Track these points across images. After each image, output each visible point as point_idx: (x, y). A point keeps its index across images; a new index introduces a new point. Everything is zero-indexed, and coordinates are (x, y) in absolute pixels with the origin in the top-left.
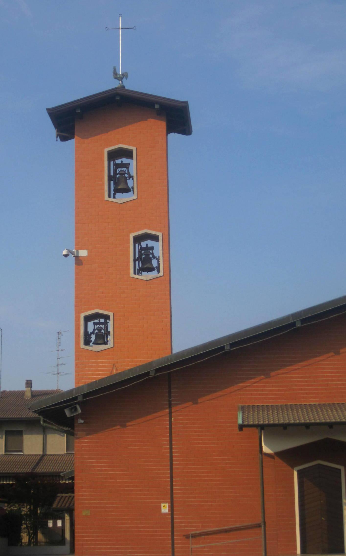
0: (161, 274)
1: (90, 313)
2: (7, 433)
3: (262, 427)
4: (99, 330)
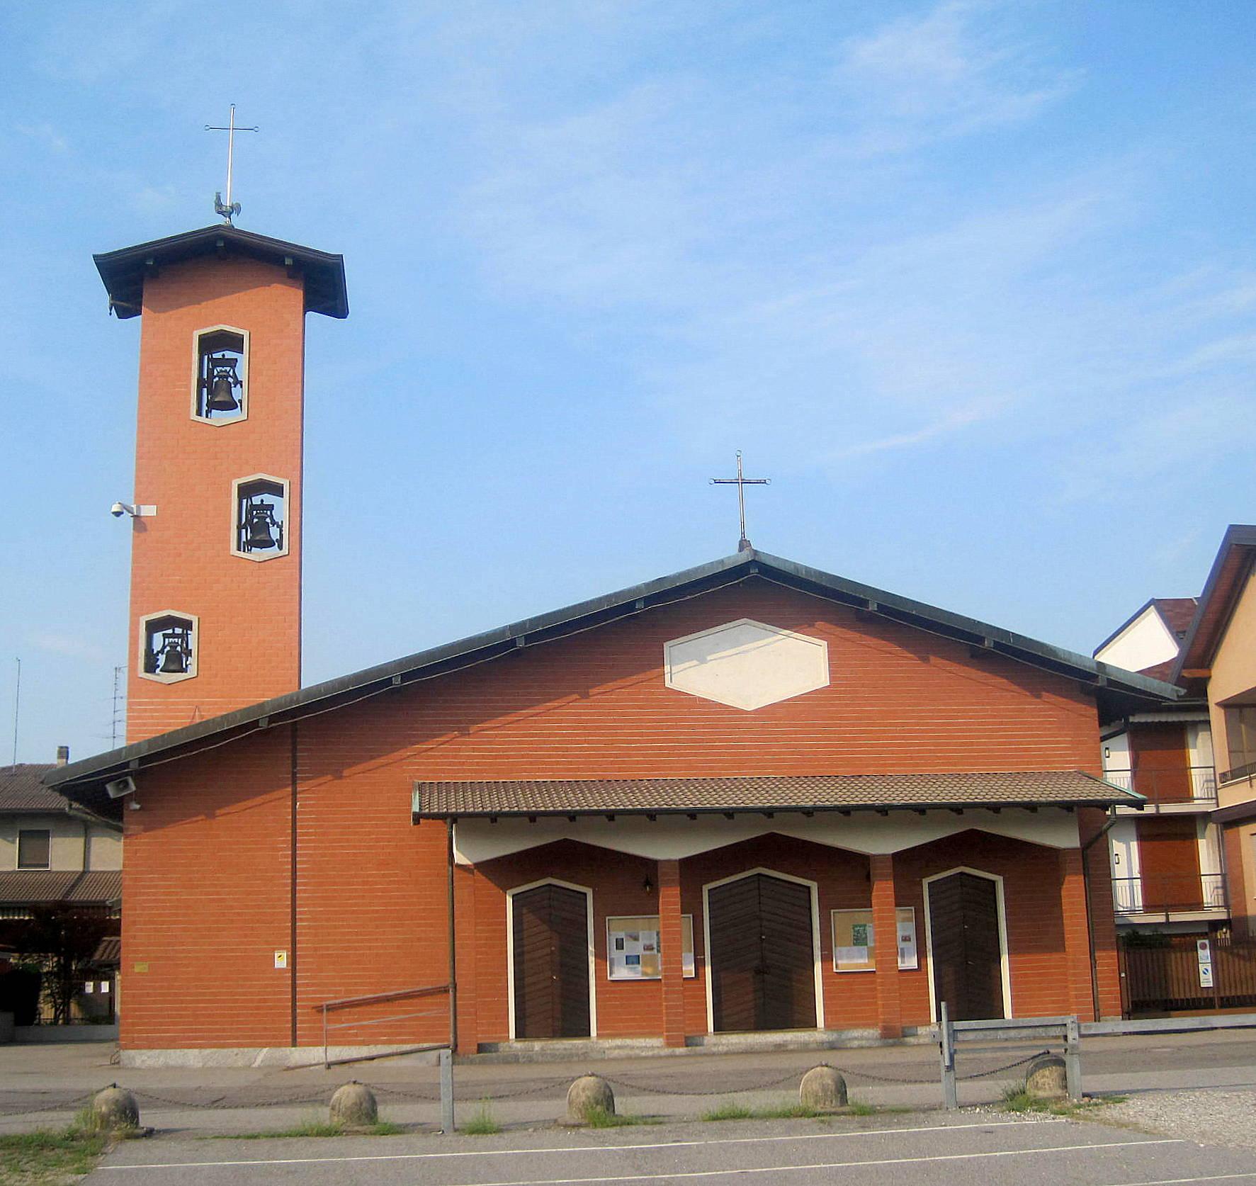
0: (285, 551)
1: (734, 1036)
2: (23, 835)
3: (454, 818)
4: (173, 646)
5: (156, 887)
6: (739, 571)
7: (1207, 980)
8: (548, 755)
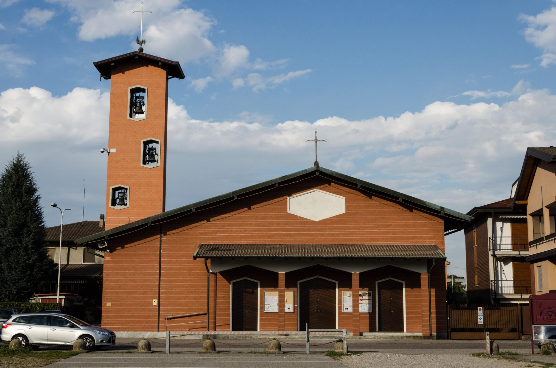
5: (114, 277)
6: (312, 173)
7: (481, 322)
8: (240, 232)
